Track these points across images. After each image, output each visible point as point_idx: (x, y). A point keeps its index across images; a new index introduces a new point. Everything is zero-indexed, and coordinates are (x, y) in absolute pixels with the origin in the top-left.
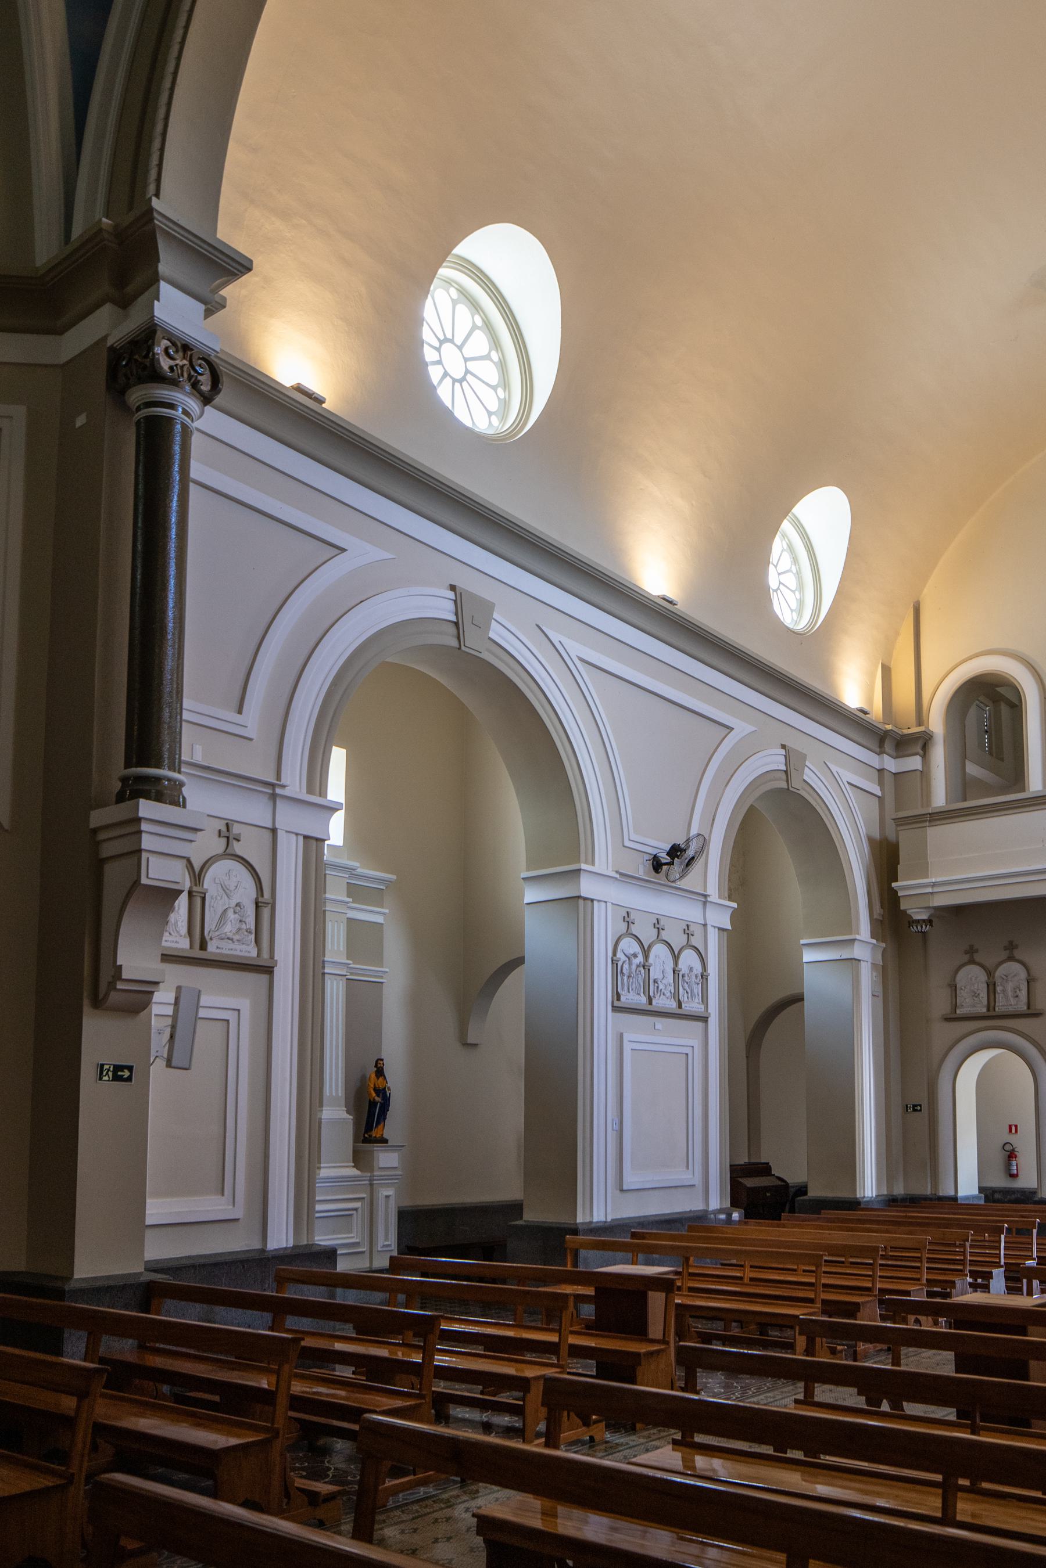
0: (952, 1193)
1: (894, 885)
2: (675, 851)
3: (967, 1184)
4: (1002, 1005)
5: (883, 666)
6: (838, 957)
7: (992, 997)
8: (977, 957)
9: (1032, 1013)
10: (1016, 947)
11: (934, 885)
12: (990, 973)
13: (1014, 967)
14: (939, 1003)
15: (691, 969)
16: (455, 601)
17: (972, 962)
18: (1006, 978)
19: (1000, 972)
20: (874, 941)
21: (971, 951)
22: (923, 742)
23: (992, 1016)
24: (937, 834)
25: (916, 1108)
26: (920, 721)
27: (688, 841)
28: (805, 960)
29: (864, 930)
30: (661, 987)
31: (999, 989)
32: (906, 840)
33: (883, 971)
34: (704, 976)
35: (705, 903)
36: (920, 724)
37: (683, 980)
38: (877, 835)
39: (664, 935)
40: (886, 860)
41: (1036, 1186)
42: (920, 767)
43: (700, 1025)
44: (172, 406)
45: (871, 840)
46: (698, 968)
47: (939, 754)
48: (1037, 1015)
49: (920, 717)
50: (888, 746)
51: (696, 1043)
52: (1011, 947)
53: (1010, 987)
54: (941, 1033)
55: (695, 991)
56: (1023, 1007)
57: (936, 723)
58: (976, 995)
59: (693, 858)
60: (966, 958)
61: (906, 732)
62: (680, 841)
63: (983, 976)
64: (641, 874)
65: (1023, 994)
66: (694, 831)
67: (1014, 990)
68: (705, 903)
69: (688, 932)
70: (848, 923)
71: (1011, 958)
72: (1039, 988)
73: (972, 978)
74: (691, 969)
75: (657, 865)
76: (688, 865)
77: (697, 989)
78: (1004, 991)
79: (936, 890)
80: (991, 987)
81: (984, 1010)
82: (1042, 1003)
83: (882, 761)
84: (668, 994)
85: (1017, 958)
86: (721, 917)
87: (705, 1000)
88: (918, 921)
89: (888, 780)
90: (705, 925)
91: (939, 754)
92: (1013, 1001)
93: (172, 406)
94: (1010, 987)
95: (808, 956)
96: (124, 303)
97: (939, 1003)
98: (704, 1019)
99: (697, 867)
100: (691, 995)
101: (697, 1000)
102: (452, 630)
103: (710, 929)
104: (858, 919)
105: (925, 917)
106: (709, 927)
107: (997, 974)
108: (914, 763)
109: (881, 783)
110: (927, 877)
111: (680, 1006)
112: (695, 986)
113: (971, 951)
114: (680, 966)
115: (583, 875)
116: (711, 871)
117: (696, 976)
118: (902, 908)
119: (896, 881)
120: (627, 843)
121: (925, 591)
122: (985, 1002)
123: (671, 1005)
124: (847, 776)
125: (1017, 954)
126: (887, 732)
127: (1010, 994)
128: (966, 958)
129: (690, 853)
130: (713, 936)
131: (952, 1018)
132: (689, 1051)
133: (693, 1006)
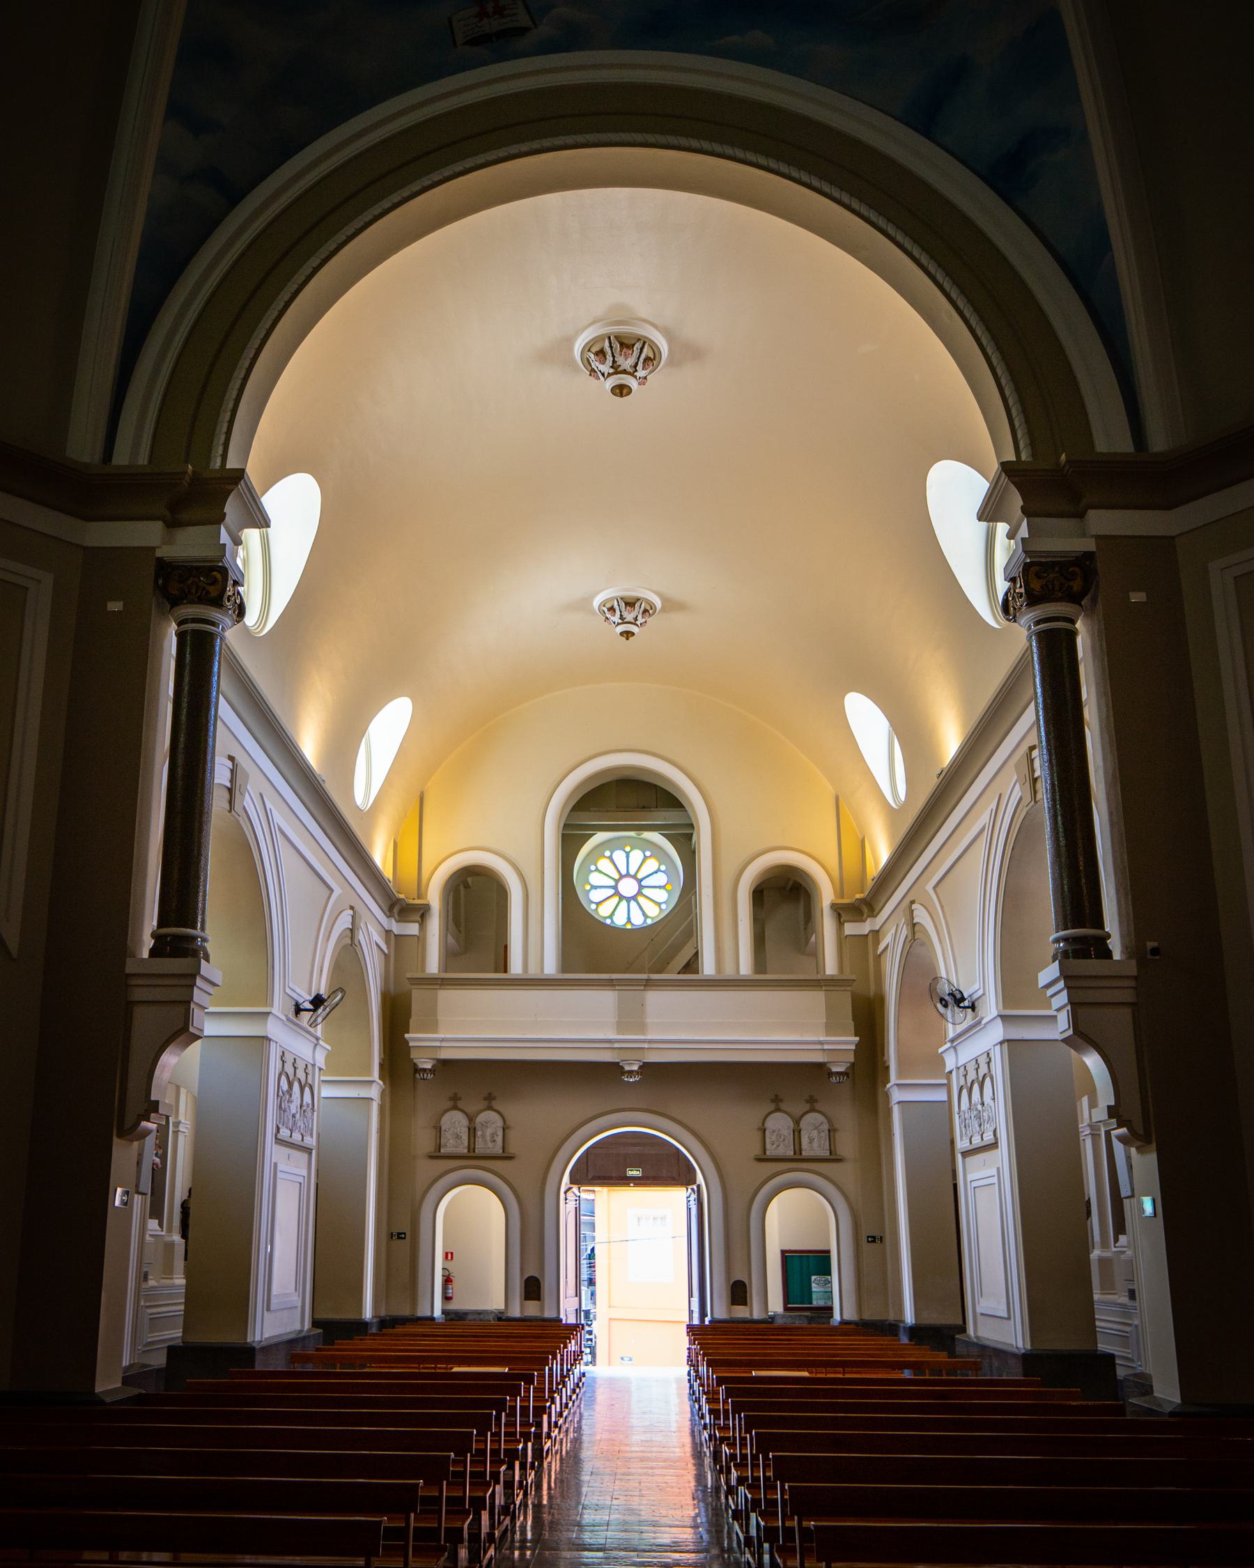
0: (429, 1314)
1: (406, 1036)
3: (368, 1313)
4: (480, 1148)
8: (460, 1104)
10: (494, 1098)
11: (443, 1040)
12: (471, 1119)
16: (232, 771)
17: (455, 1108)
18: (485, 1125)
19: (481, 1118)
21: (455, 1098)
22: (423, 913)
23: (798, 1158)
25: (401, 1236)
31: (479, 1133)
32: (418, 997)
41: (502, 1307)
44: (213, 624)
48: (510, 1158)
49: (421, 891)
52: (490, 1098)
53: (489, 1132)
54: (425, 1169)
56: (498, 1150)
57: (434, 897)
58: (458, 1137)
60: (450, 1104)
61: (411, 901)
63: (465, 1122)
65: (499, 1139)
67: (493, 1135)
71: (490, 1108)
72: (512, 1134)
73: (455, 1122)
75: (298, 1010)
78: (483, 1136)
80: (472, 1131)
82: (512, 1150)
88: (425, 1070)
90: (314, 1065)
91: (435, 925)
92: (490, 1145)
93: (213, 624)
94: (489, 1132)
96: (173, 524)
97: (423, 1141)
105: (429, 1066)
108: (413, 929)
109: (387, 942)
110: (436, 1033)
113: (455, 1098)
120: (288, 991)
125: (495, 1104)
126: (399, 900)
128: (450, 1104)
131: (436, 1156)
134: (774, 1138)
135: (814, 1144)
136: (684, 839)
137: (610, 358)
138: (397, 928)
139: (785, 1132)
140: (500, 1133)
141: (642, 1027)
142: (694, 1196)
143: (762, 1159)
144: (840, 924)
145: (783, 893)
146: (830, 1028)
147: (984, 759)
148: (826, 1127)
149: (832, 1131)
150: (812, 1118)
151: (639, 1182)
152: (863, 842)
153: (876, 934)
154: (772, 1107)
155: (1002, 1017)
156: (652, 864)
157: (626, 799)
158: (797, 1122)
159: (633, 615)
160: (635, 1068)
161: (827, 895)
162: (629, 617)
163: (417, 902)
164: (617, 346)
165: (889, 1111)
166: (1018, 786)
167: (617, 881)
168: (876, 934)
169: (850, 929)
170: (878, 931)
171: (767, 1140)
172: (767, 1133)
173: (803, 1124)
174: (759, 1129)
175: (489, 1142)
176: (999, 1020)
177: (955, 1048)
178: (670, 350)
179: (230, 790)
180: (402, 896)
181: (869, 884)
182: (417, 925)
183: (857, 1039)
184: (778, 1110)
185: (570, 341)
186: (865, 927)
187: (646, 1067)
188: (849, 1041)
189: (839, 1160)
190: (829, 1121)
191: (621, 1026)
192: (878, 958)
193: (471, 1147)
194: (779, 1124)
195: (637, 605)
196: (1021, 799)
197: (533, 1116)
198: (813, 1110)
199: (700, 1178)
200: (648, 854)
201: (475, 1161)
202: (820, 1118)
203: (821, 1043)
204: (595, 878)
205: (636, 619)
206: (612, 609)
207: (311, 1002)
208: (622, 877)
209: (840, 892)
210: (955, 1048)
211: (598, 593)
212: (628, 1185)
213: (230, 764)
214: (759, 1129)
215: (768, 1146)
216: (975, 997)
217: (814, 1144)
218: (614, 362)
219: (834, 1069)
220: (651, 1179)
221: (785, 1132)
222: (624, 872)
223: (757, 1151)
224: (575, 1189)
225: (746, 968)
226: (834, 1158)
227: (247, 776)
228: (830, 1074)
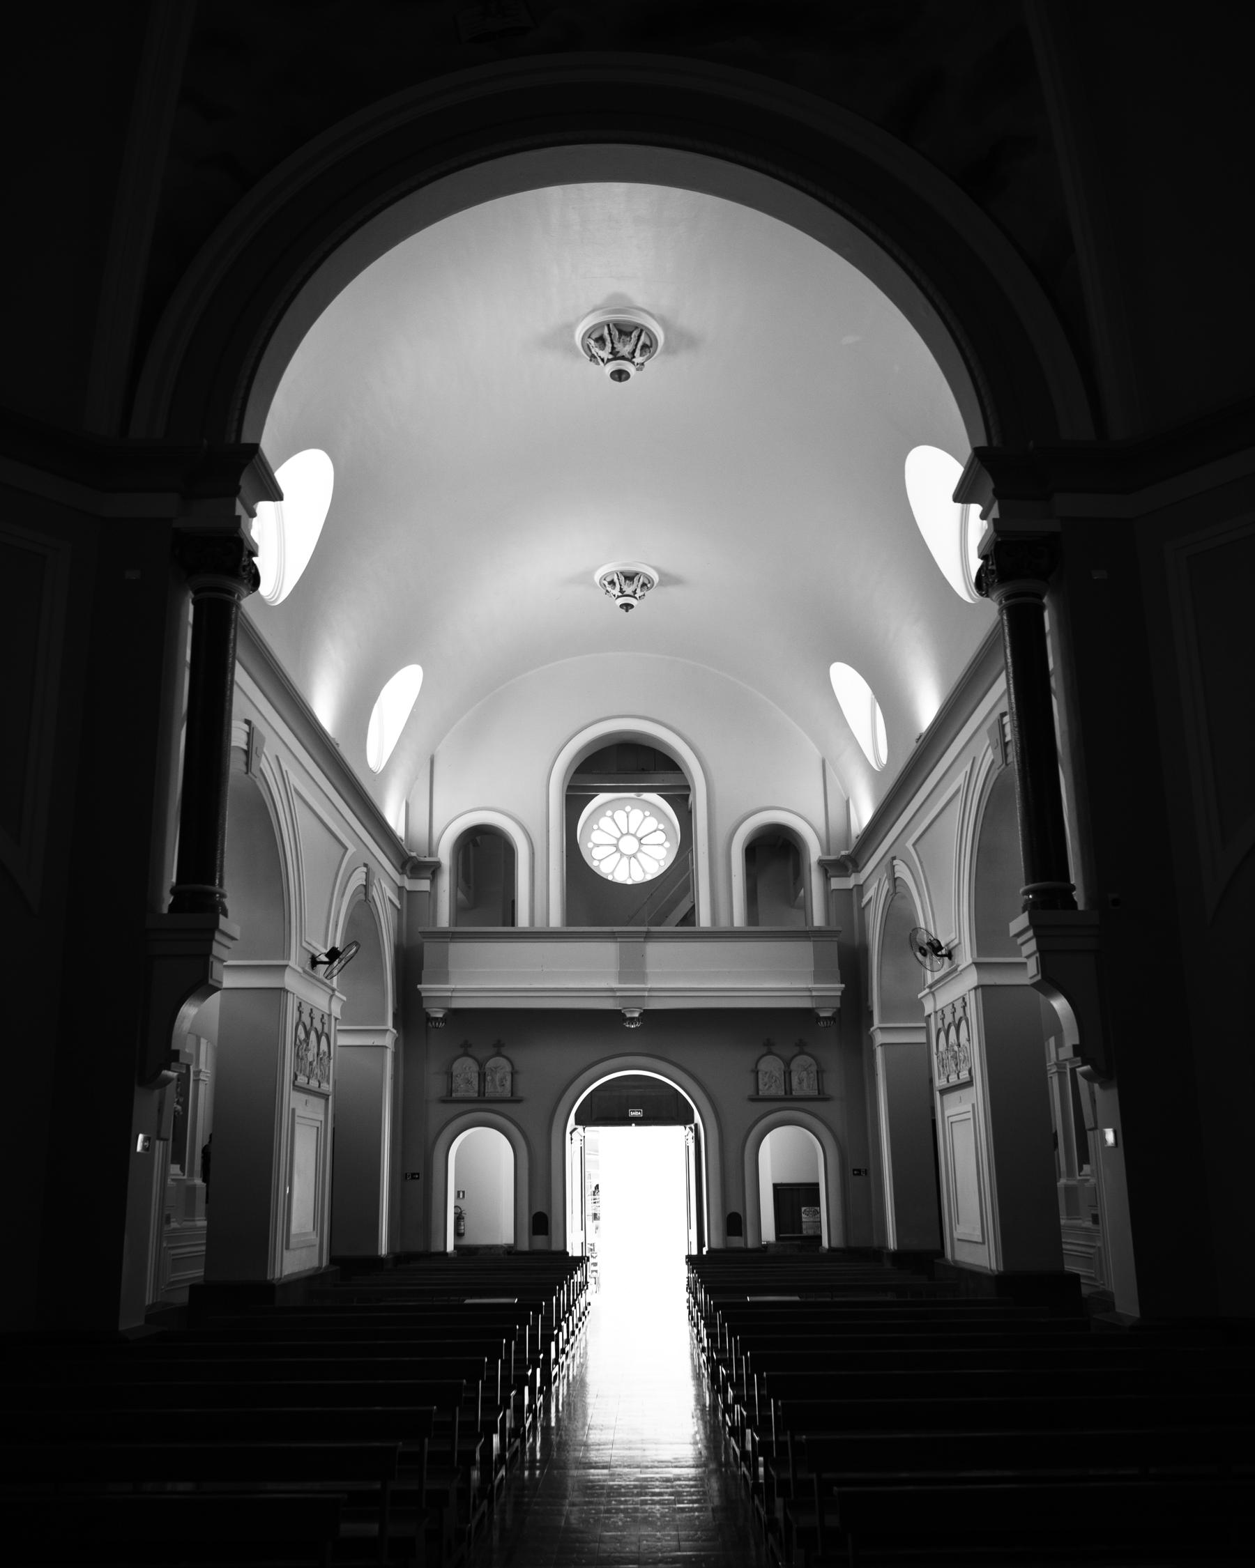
0: (442, 1249)
4: (490, 1091)
9: (515, 1100)
12: (481, 1065)
13: (501, 1061)
16: (248, 734)
17: (466, 1054)
18: (495, 1070)
22: (433, 870)
23: (788, 1098)
25: (414, 1176)
31: (489, 1078)
32: (430, 950)
36: (430, 855)
48: (519, 1101)
50: (408, 868)
54: (437, 1113)
57: (444, 855)
58: (469, 1082)
63: (475, 1068)
65: (508, 1084)
67: (501, 1080)
71: (499, 1054)
73: (465, 1068)
78: (493, 1080)
80: (482, 1076)
82: (520, 1093)
88: (437, 1019)
89: (405, 895)
90: (330, 1015)
91: (445, 882)
92: (499, 1089)
94: (498, 1077)
102: (243, 757)
105: (440, 1015)
108: (424, 885)
109: (400, 898)
115: (288, 970)
120: (304, 944)
125: (504, 1051)
131: (448, 1099)
135: (803, 1083)
136: (681, 800)
138: (408, 884)
140: (509, 1078)
141: (643, 977)
143: (756, 1099)
144: (827, 879)
145: (774, 850)
146: (818, 977)
148: (814, 1068)
150: (803, 1060)
151: (640, 1122)
153: (860, 888)
154: (764, 1050)
157: (625, 762)
158: (788, 1064)
160: (636, 1015)
161: (815, 852)
162: (629, 590)
163: (428, 859)
166: (990, 750)
167: (618, 840)
168: (860, 888)
169: (836, 883)
172: (760, 1076)
173: (793, 1066)
175: (499, 1084)
177: (933, 993)
180: (414, 854)
181: (854, 841)
184: (770, 1053)
185: (570, 328)
186: (850, 882)
187: (648, 1015)
189: (826, 1099)
191: (622, 977)
192: (862, 910)
193: (481, 1092)
194: (771, 1066)
195: (635, 334)
197: (541, 1060)
198: (802, 1053)
201: (485, 1106)
202: (810, 1060)
203: (810, 990)
205: (635, 592)
207: (327, 955)
208: (623, 835)
209: (827, 848)
210: (933, 993)
212: (630, 1125)
216: (952, 945)
217: (803, 1083)
218: (613, 348)
219: (822, 1014)
223: (750, 1091)
224: (580, 1128)
225: (739, 920)
226: (822, 1097)
227: (263, 739)
228: (819, 1019)
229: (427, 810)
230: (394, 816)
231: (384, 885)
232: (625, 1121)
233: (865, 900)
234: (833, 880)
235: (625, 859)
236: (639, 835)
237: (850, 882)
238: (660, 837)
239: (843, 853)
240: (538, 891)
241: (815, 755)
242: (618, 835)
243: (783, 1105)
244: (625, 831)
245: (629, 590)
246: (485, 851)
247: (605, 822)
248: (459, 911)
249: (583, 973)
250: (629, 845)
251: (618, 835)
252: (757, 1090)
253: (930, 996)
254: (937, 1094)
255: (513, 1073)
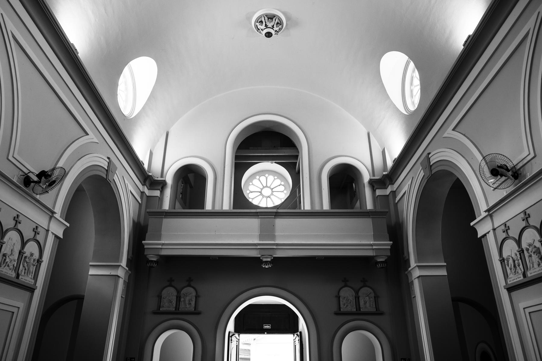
1: (143, 242)
2: (43, 174)
4: (182, 307)
5: (151, 151)
6: (109, 274)
7: (178, 303)
9: (196, 313)
11: (163, 244)
12: (179, 292)
13: (191, 290)
14: (151, 304)
15: (32, 255)
17: (170, 285)
19: (184, 291)
20: (127, 269)
22: (162, 185)
23: (358, 313)
24: (167, 222)
26: (162, 176)
27: (54, 169)
28: (90, 273)
29: (124, 263)
30: (8, 260)
31: (182, 299)
32: (152, 221)
33: (128, 285)
34: (39, 261)
35: (51, 217)
37: (25, 261)
38: (136, 220)
39: (20, 227)
40: (140, 231)
42: (159, 195)
43: (28, 294)
45: (134, 221)
46: (36, 255)
47: (168, 192)
48: (199, 313)
50: (147, 183)
51: (21, 305)
52: (190, 280)
55: (31, 270)
57: (169, 179)
58: (170, 302)
59: (54, 182)
61: (156, 179)
62: (47, 169)
63: (175, 293)
64: (15, 180)
65: (193, 303)
66: (60, 164)
67: (190, 300)
68: (51, 217)
69: (36, 230)
70: (118, 258)
71: (189, 286)
73: (170, 293)
74: (32, 255)
76: (50, 185)
77: (33, 269)
78: (184, 301)
79: (164, 247)
80: (178, 298)
81: (174, 309)
82: (200, 309)
83: (144, 188)
84: (11, 267)
85: (192, 285)
86: (57, 230)
87: (36, 278)
88: (152, 261)
89: (145, 198)
90: (48, 231)
91: (168, 192)
92: (188, 306)
94: (187, 299)
95: (92, 272)
98: (31, 290)
99: (52, 192)
100: (27, 272)
101: (30, 276)
103: (50, 234)
104: (122, 256)
105: (155, 259)
106: (50, 232)
107: (182, 292)
108: (157, 193)
109: (141, 198)
111: (18, 276)
112: (32, 266)
114: (25, 250)
116: (60, 197)
117: (34, 260)
118: (145, 254)
119: (145, 240)
120: (10, 158)
121: (171, 129)
122: (174, 305)
123: (12, 274)
124: (131, 188)
127: (187, 302)
129: (53, 178)
130: (51, 239)
132: (15, 310)
133: (27, 279)
134: (345, 301)
135: (367, 304)
136: (292, 166)
137: (264, 23)
138: (147, 192)
139: (351, 298)
140: (194, 300)
141: (273, 237)
142: (298, 338)
143: (339, 313)
145: (344, 180)
146: (376, 237)
147: (419, 143)
148: (373, 295)
149: (376, 297)
150: (365, 290)
151: (269, 332)
152: (384, 149)
153: (394, 193)
155: (418, 266)
156: (278, 182)
157: (266, 142)
158: (357, 292)
159: (272, 24)
160: (269, 260)
161: (366, 177)
162: (270, 25)
163: (160, 179)
164: (266, 18)
165: (409, 286)
166: (422, 171)
167: (262, 189)
168: (394, 193)
169: (379, 192)
170: (395, 192)
171: (341, 302)
172: (341, 299)
173: (360, 294)
174: (336, 297)
175: (187, 304)
176: (417, 268)
178: (287, 24)
179: (107, 171)
180: (150, 174)
181: (390, 163)
182: (159, 192)
183: (392, 242)
184: (346, 286)
185: (249, 18)
186: (388, 191)
187: (276, 261)
188: (386, 244)
189: (382, 314)
190: (374, 292)
191: (261, 237)
192: (396, 205)
193: (177, 307)
194: (347, 293)
195: (274, 19)
196: (424, 176)
197: (213, 290)
198: (365, 286)
199: (302, 325)
200: (276, 177)
201: (178, 316)
202: (370, 290)
203: (371, 245)
204: (251, 188)
205: (273, 26)
206: (261, 22)
207: (38, 176)
208: (264, 187)
211: (255, 13)
212: (264, 333)
213: (108, 160)
214: (336, 297)
215: (342, 306)
217: (367, 304)
218: (266, 24)
219: (379, 260)
220: (276, 330)
221: (351, 298)
222: (265, 185)
224: (237, 335)
225: (326, 206)
226: (378, 313)
227: (116, 168)
228: (377, 263)
229: (167, 164)
230: (142, 154)
231: (126, 182)
232: (261, 331)
233: (397, 199)
234: (377, 190)
235: (265, 199)
236: (272, 187)
237: (388, 191)
238: (282, 188)
239: (384, 173)
240: (218, 194)
241: (364, 132)
242: (262, 187)
243: (356, 317)
244: (265, 185)
245: (270, 25)
246: (191, 180)
247: (255, 182)
248: (173, 204)
249: (238, 237)
250: (267, 192)
251: (262, 187)
252: (340, 308)
253: (489, 218)
254: (504, 294)
255: (197, 297)
